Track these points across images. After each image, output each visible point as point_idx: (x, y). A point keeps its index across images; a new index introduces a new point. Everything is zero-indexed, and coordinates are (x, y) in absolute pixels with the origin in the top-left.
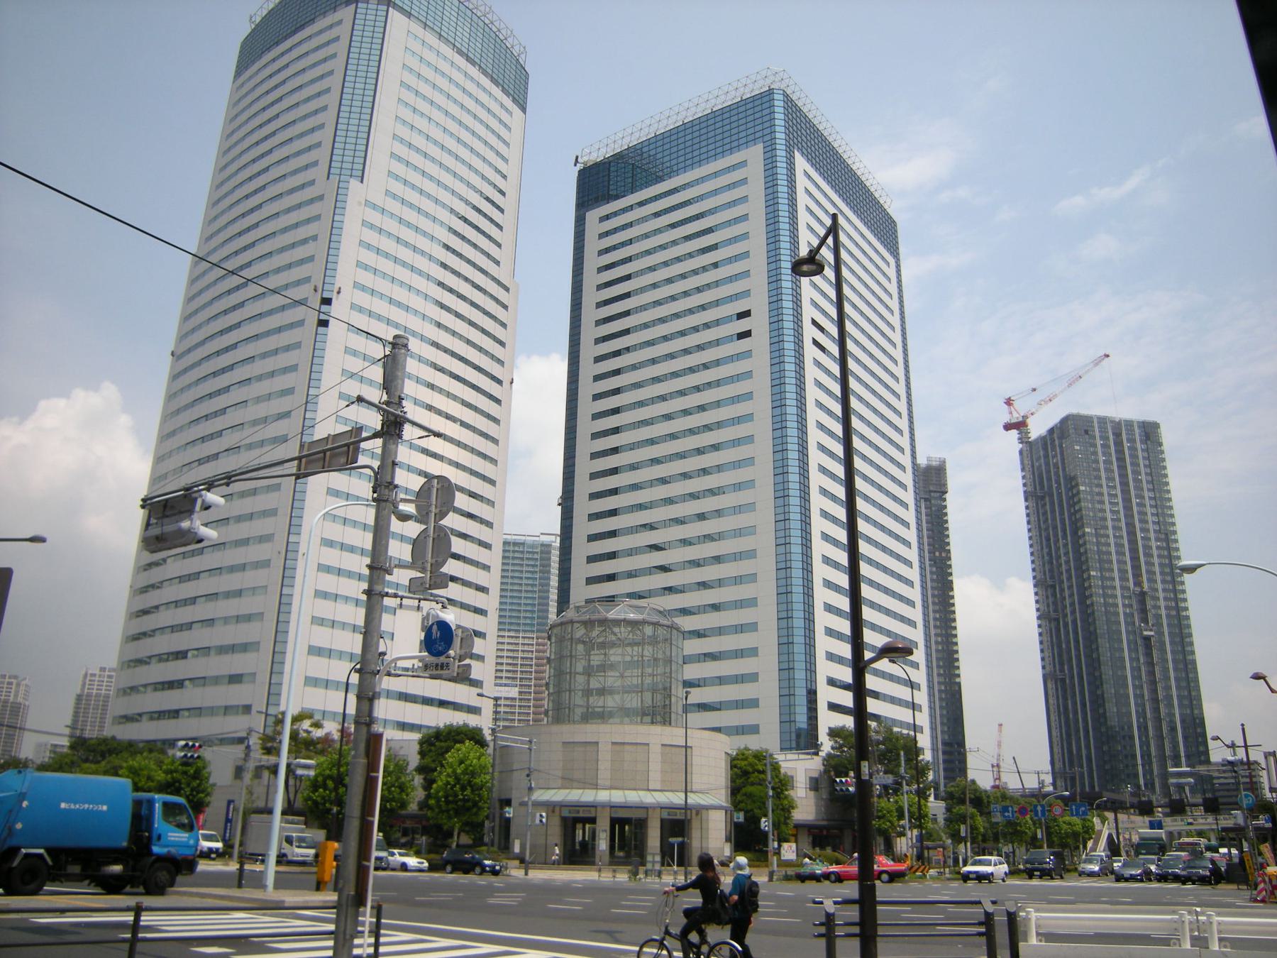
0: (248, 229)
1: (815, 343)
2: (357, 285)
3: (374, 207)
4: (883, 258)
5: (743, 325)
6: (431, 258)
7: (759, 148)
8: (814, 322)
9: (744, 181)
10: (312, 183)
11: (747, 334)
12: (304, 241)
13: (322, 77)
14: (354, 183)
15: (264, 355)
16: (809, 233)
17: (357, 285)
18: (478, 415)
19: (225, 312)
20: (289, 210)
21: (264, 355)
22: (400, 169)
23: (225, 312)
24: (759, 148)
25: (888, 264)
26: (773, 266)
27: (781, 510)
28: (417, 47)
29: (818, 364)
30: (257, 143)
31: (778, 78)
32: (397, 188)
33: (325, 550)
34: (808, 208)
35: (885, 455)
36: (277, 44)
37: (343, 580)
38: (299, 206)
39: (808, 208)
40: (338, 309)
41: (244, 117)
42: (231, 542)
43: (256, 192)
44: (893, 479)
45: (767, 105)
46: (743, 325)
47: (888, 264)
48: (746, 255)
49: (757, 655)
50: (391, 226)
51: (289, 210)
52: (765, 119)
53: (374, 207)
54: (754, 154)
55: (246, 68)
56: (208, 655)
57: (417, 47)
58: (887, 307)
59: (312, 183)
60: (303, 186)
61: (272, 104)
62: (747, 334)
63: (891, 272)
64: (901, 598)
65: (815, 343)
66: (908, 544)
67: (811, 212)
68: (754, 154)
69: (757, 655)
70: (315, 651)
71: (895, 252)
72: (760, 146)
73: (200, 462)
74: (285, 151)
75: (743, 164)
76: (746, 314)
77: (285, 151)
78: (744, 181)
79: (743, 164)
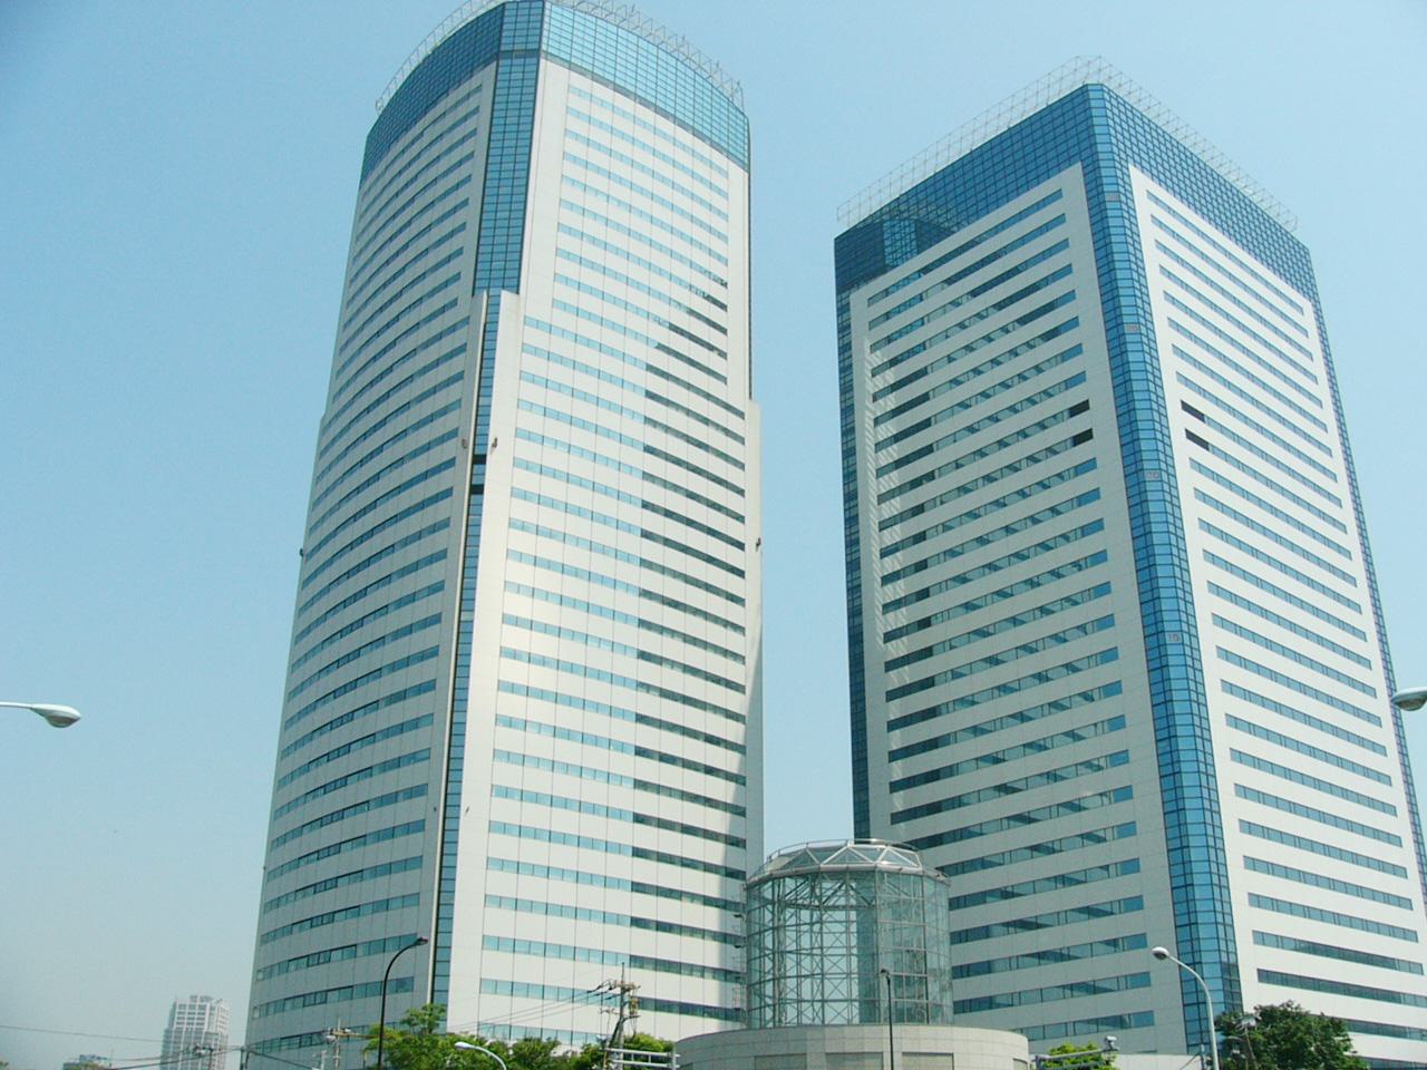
0: (381, 376)
1: (1191, 436)
2: (518, 433)
3: (537, 324)
4: (1291, 303)
5: (1079, 424)
6: (606, 882)
7: (1077, 168)
8: (1186, 407)
9: (1064, 244)
10: (454, 303)
11: (1086, 436)
12: (444, 411)
13: (449, 259)
14: (506, 296)
15: (406, 542)
16: (1164, 279)
17: (518, 433)
18: (689, 557)
19: (358, 490)
20: (426, 345)
21: (406, 542)
22: (570, 269)
23: (358, 490)
24: (1077, 168)
25: (1301, 310)
26: (1118, 361)
27: (1170, 795)
28: (582, 105)
29: (1199, 467)
30: (378, 334)
31: (1093, 69)
32: (568, 295)
33: (499, 802)
34: (1159, 245)
35: (1359, 798)
36: (406, 130)
37: (529, 806)
38: (440, 336)
39: (1159, 245)
40: (496, 474)
41: (369, 252)
42: (421, 346)
43: (372, 455)
44: (1352, 682)
45: (1081, 108)
46: (1079, 424)
47: (1301, 310)
48: (1067, 270)
49: (1138, 870)
50: (563, 347)
51: (426, 345)
52: (1079, 119)
53: (537, 324)
54: (1071, 180)
55: (373, 168)
56: (362, 879)
57: (582, 105)
58: (1310, 396)
59: (454, 303)
60: (443, 310)
61: (391, 301)
62: (1086, 436)
63: (1308, 320)
64: (1382, 866)
65: (1191, 436)
66: (1380, 749)
67: (1173, 301)
68: (1071, 180)
69: (1138, 870)
70: (497, 827)
71: (1306, 285)
72: (1078, 166)
73: (321, 821)
74: (422, 244)
75: (1057, 195)
76: (1080, 408)
77: (422, 244)
78: (1064, 244)
79: (1057, 195)
